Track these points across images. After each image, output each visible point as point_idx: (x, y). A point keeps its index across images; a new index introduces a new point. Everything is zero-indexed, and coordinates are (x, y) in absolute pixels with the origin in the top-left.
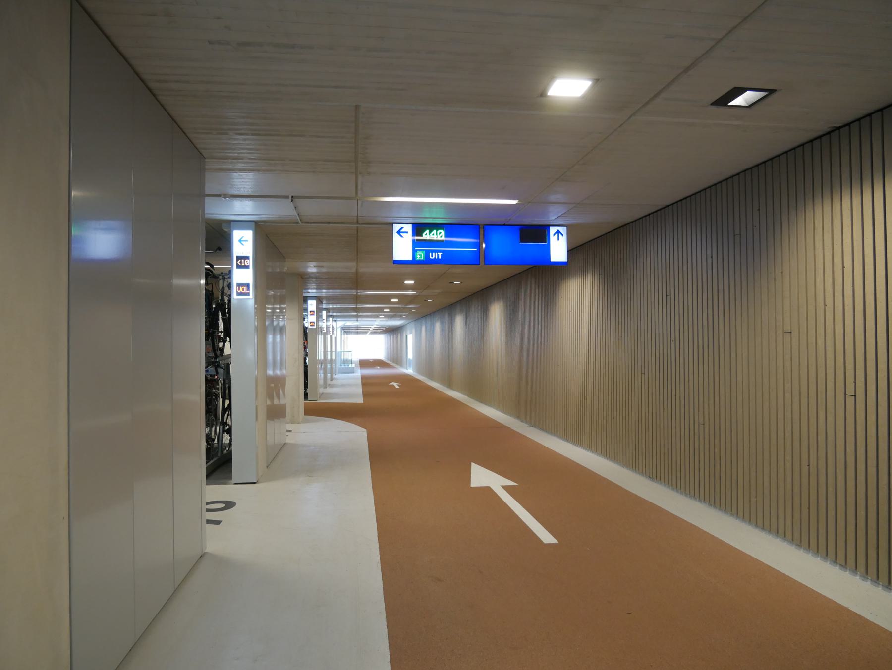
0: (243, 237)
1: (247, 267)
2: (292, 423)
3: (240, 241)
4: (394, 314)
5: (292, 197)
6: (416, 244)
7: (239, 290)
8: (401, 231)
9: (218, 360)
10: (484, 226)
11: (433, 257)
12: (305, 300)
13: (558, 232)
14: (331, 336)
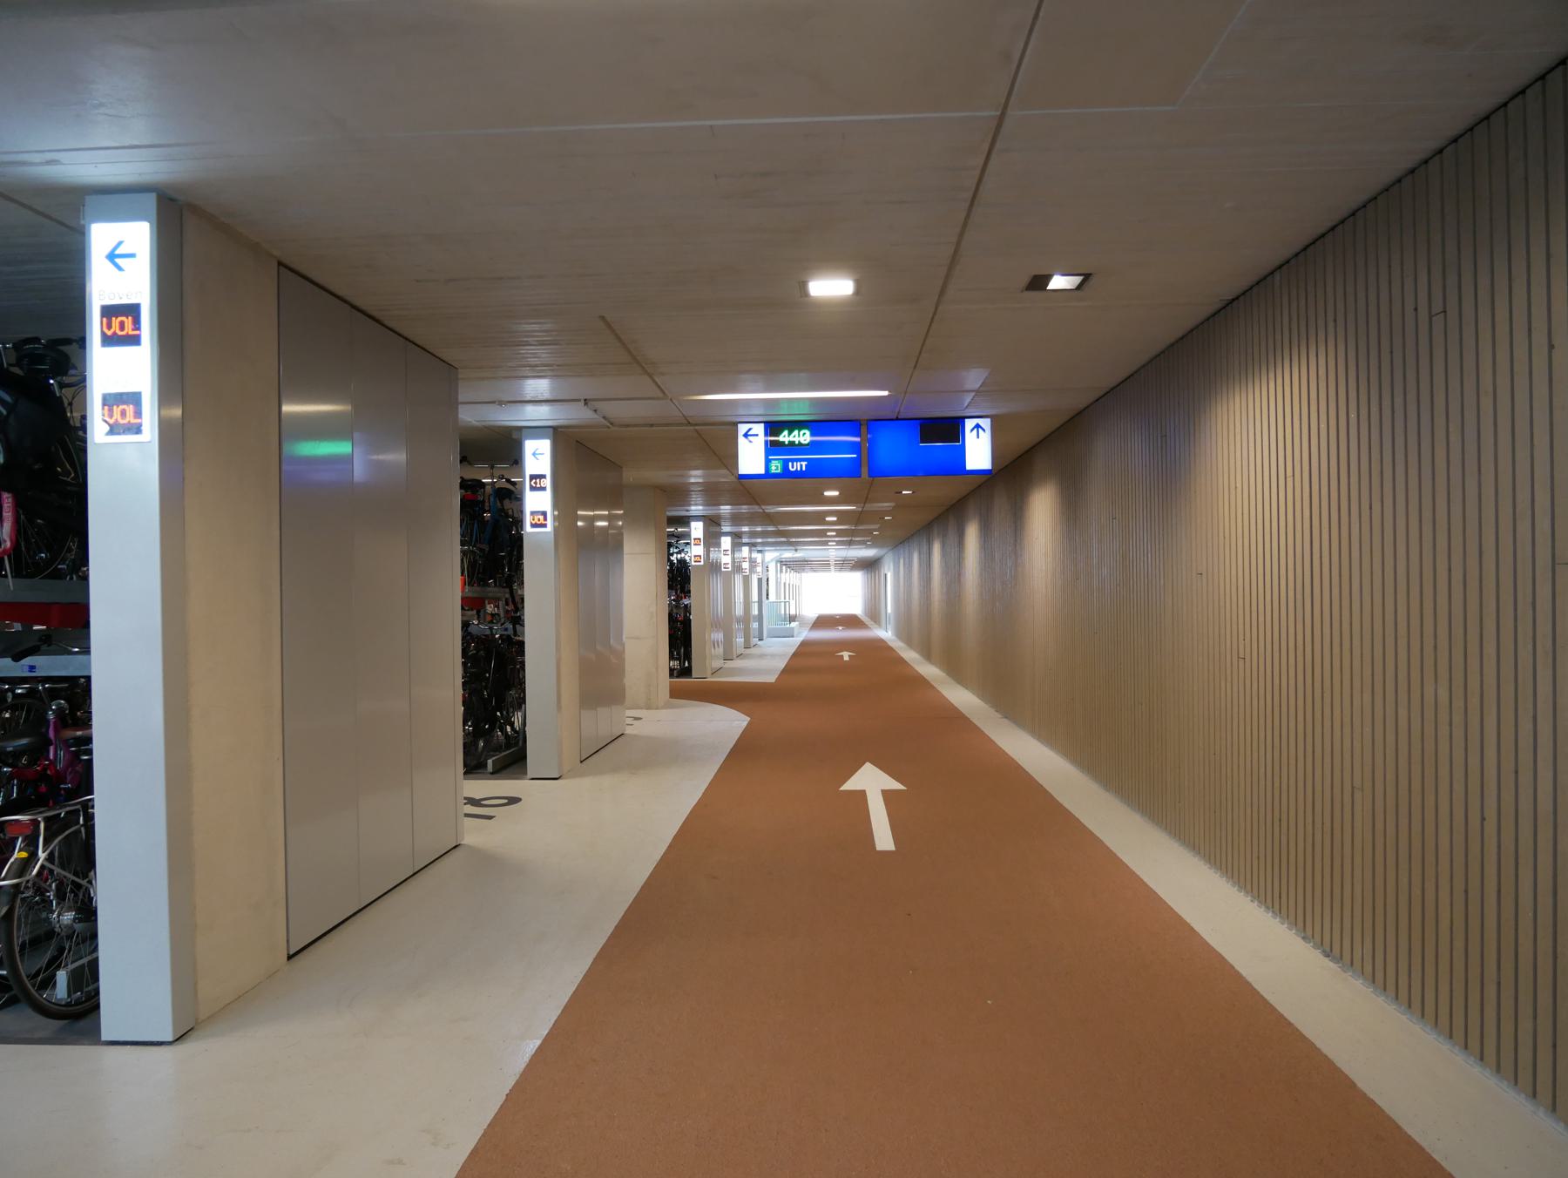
0: (120, 243)
1: (544, 489)
2: (649, 708)
3: (112, 257)
4: (849, 539)
5: (585, 400)
6: (773, 448)
7: (109, 327)
8: (749, 433)
9: (518, 614)
10: (869, 420)
11: (794, 469)
12: (685, 521)
13: (978, 426)
14: (747, 580)
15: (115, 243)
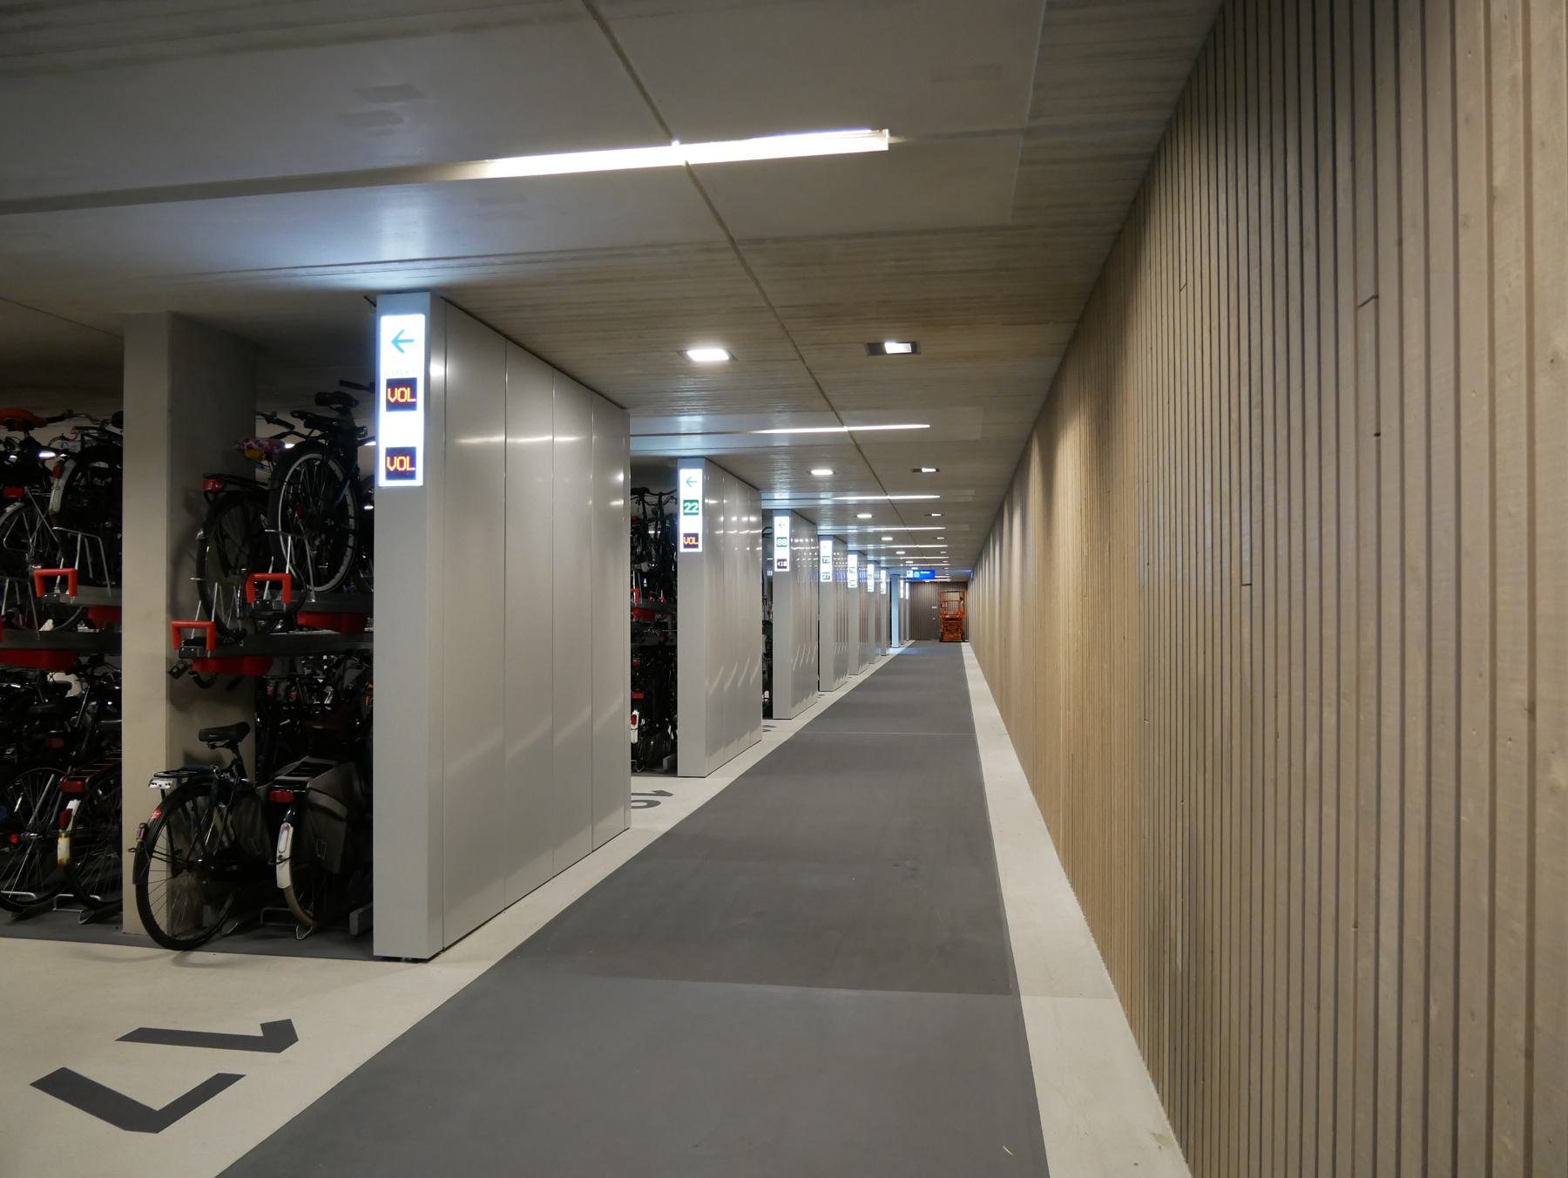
0: (402, 331)
3: (396, 342)
7: (392, 464)
15: (399, 331)
